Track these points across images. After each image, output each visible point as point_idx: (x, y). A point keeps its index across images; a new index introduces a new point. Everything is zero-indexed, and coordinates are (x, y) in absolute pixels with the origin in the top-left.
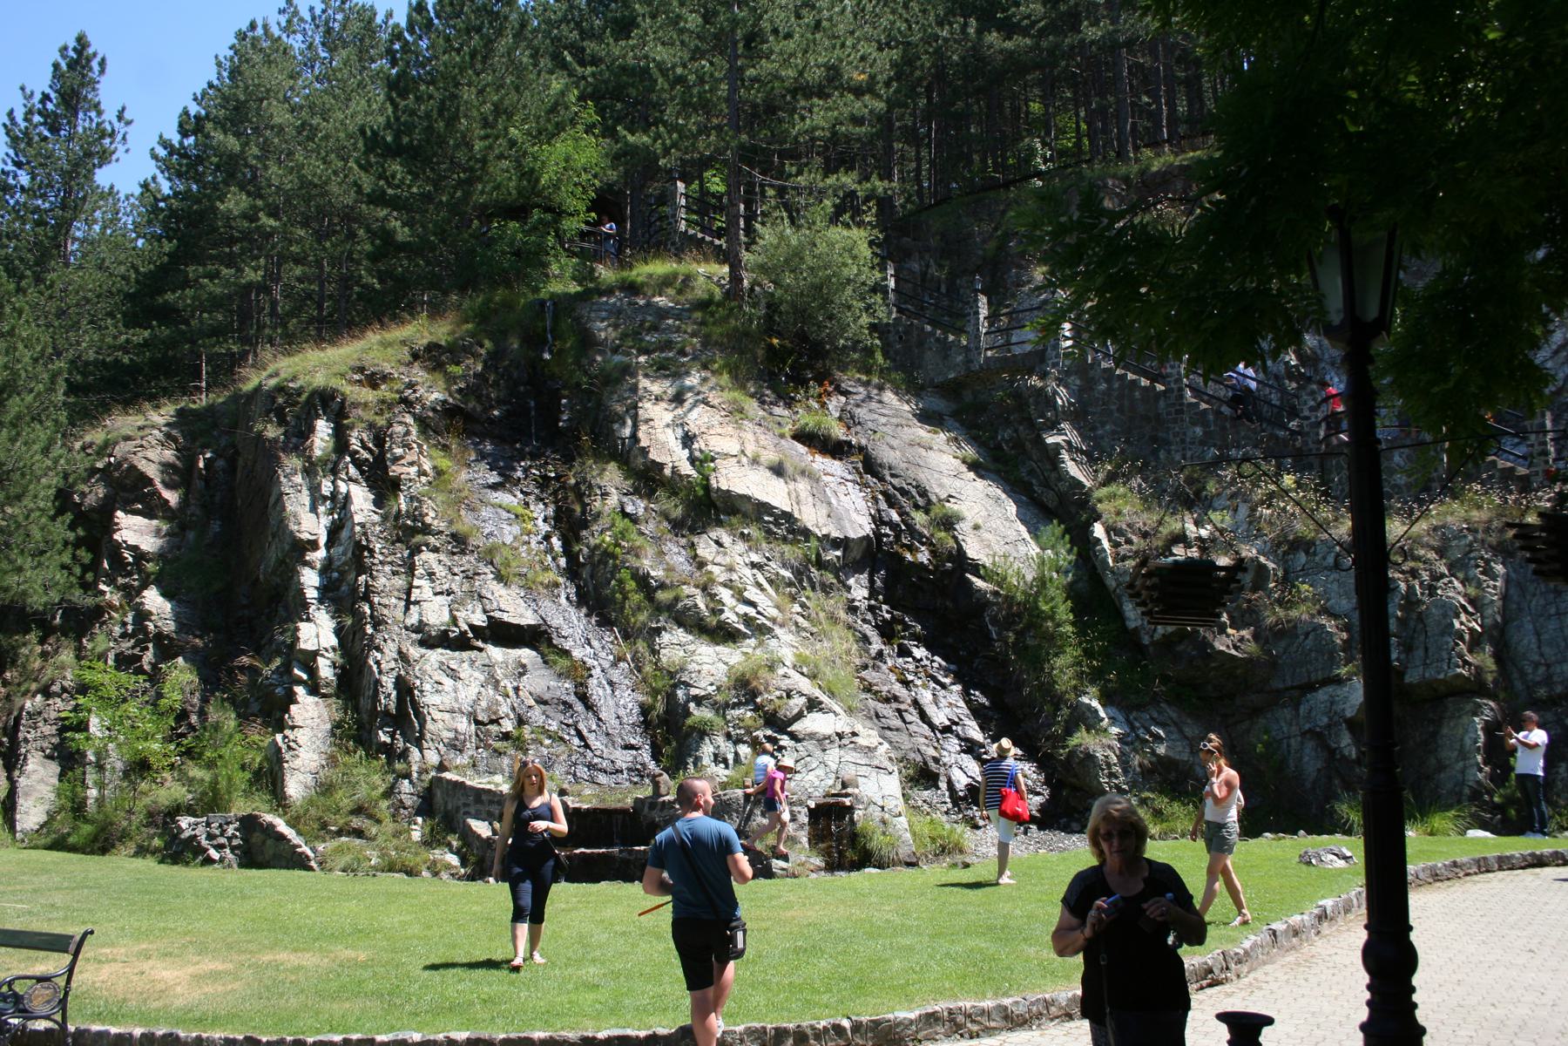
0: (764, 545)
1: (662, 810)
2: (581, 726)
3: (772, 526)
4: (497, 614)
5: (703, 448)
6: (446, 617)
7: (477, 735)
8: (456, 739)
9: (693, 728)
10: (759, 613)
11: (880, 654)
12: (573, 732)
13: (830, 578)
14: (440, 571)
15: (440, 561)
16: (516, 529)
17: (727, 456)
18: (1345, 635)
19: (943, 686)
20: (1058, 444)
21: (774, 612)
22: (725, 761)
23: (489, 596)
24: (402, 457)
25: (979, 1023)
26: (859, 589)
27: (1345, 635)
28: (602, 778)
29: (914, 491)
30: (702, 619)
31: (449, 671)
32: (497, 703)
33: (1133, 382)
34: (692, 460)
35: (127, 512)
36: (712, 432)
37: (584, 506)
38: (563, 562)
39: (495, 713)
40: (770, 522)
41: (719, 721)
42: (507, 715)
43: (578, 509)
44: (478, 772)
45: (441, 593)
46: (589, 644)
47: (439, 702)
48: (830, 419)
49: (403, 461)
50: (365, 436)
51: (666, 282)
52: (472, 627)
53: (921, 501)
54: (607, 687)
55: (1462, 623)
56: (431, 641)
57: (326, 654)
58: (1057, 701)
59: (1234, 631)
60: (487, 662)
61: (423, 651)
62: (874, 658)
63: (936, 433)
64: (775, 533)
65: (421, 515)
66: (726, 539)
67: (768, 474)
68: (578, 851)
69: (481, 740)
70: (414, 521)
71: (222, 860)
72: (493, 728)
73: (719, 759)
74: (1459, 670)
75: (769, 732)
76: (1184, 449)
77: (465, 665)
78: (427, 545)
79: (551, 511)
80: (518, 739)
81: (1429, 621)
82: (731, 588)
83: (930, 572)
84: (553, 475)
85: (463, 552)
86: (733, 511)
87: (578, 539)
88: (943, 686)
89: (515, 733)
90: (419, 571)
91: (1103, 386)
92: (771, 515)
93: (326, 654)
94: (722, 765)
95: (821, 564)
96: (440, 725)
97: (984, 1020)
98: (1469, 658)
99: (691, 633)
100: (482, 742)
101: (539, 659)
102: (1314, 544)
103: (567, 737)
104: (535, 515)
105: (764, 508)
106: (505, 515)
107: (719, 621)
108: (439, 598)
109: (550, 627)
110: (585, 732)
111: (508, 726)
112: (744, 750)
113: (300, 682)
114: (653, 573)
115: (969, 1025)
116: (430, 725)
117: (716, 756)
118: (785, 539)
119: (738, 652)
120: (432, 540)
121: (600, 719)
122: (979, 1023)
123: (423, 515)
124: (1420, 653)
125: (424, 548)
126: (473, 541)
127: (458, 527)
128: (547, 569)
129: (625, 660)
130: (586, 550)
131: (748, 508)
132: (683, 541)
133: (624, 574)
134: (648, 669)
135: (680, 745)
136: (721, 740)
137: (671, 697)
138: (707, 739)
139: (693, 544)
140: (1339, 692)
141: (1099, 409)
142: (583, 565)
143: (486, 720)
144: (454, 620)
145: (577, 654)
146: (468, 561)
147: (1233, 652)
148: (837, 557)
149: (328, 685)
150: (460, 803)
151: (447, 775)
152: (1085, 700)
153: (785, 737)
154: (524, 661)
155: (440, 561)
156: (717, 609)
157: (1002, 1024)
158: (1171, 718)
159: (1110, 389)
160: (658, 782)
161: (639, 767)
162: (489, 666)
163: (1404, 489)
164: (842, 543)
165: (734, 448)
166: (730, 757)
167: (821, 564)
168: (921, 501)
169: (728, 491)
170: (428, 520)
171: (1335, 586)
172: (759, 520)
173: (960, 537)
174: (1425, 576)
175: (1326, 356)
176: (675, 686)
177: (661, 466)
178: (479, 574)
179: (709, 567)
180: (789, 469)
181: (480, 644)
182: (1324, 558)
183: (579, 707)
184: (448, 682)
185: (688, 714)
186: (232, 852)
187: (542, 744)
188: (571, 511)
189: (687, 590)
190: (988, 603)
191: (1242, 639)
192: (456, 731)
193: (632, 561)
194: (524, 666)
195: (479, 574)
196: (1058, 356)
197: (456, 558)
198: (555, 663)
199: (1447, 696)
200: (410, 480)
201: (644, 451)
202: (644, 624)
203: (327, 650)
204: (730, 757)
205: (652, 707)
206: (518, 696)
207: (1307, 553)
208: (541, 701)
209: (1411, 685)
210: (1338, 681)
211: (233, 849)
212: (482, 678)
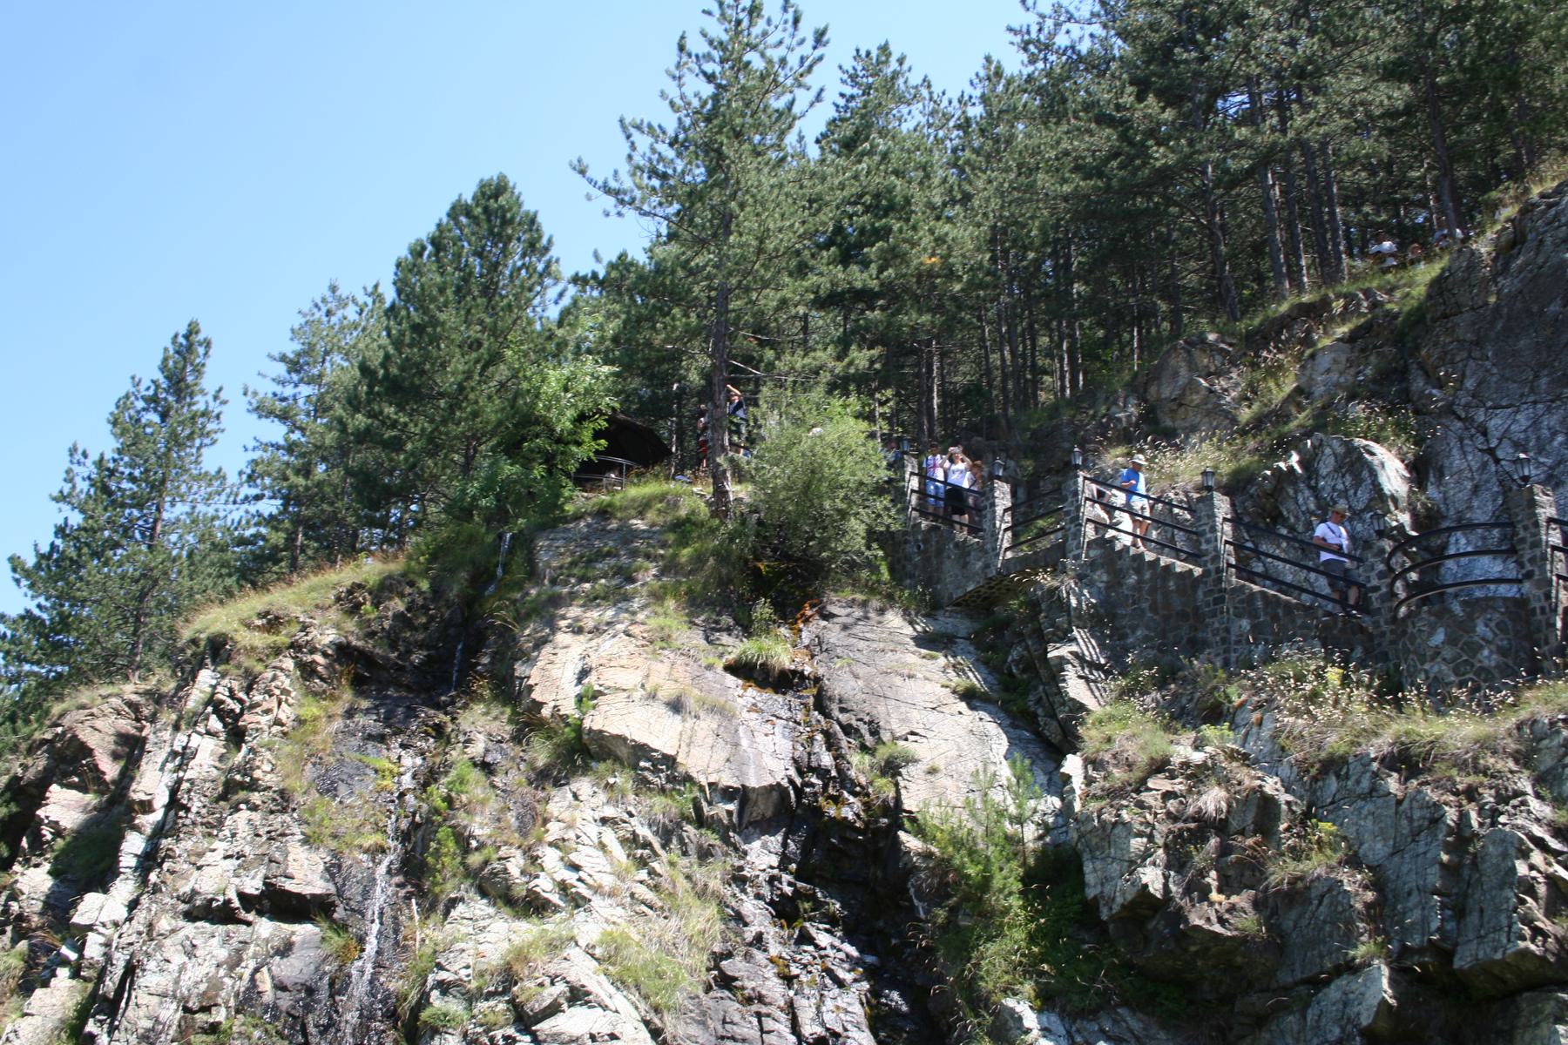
0: (631, 797)
3: (646, 773)
8: (153, 1029)
11: (759, 940)
13: (711, 838)
18: (1370, 896)
19: (840, 984)
20: (1061, 658)
24: (258, 705)
26: (763, 854)
27: (1370, 896)
29: (864, 729)
33: (1168, 568)
35: (63, 785)
45: (230, 857)
48: (781, 651)
50: (236, 685)
51: (643, 507)
52: (242, 896)
53: (869, 740)
55: (1532, 867)
57: (102, 930)
58: (979, 1002)
59: (1222, 897)
62: (750, 944)
63: (933, 658)
67: (663, 710)
74: (1522, 944)
76: (1226, 651)
78: (247, 802)
81: (1486, 866)
83: (858, 831)
88: (840, 984)
91: (1132, 579)
92: (649, 760)
93: (102, 930)
96: (142, 1012)
98: (1543, 923)
102: (1347, 763)
105: (642, 750)
113: (65, 962)
118: (663, 790)
124: (1474, 919)
131: (623, 752)
140: (1354, 987)
141: (1129, 610)
143: (196, 1007)
147: (1217, 928)
148: (729, 813)
152: (1010, 1002)
158: (1132, 1032)
159: (1140, 581)
163: (1496, 673)
164: (741, 795)
167: (701, 821)
168: (869, 740)
169: (601, 732)
170: (257, 774)
171: (1369, 822)
173: (902, 784)
174: (1488, 797)
175: (1452, 512)
180: (691, 703)
182: (1358, 782)
190: (914, 869)
191: (1232, 909)
196: (1079, 546)
199: (1519, 991)
203: (104, 925)
207: (1338, 776)
209: (1461, 970)
210: (1352, 968)
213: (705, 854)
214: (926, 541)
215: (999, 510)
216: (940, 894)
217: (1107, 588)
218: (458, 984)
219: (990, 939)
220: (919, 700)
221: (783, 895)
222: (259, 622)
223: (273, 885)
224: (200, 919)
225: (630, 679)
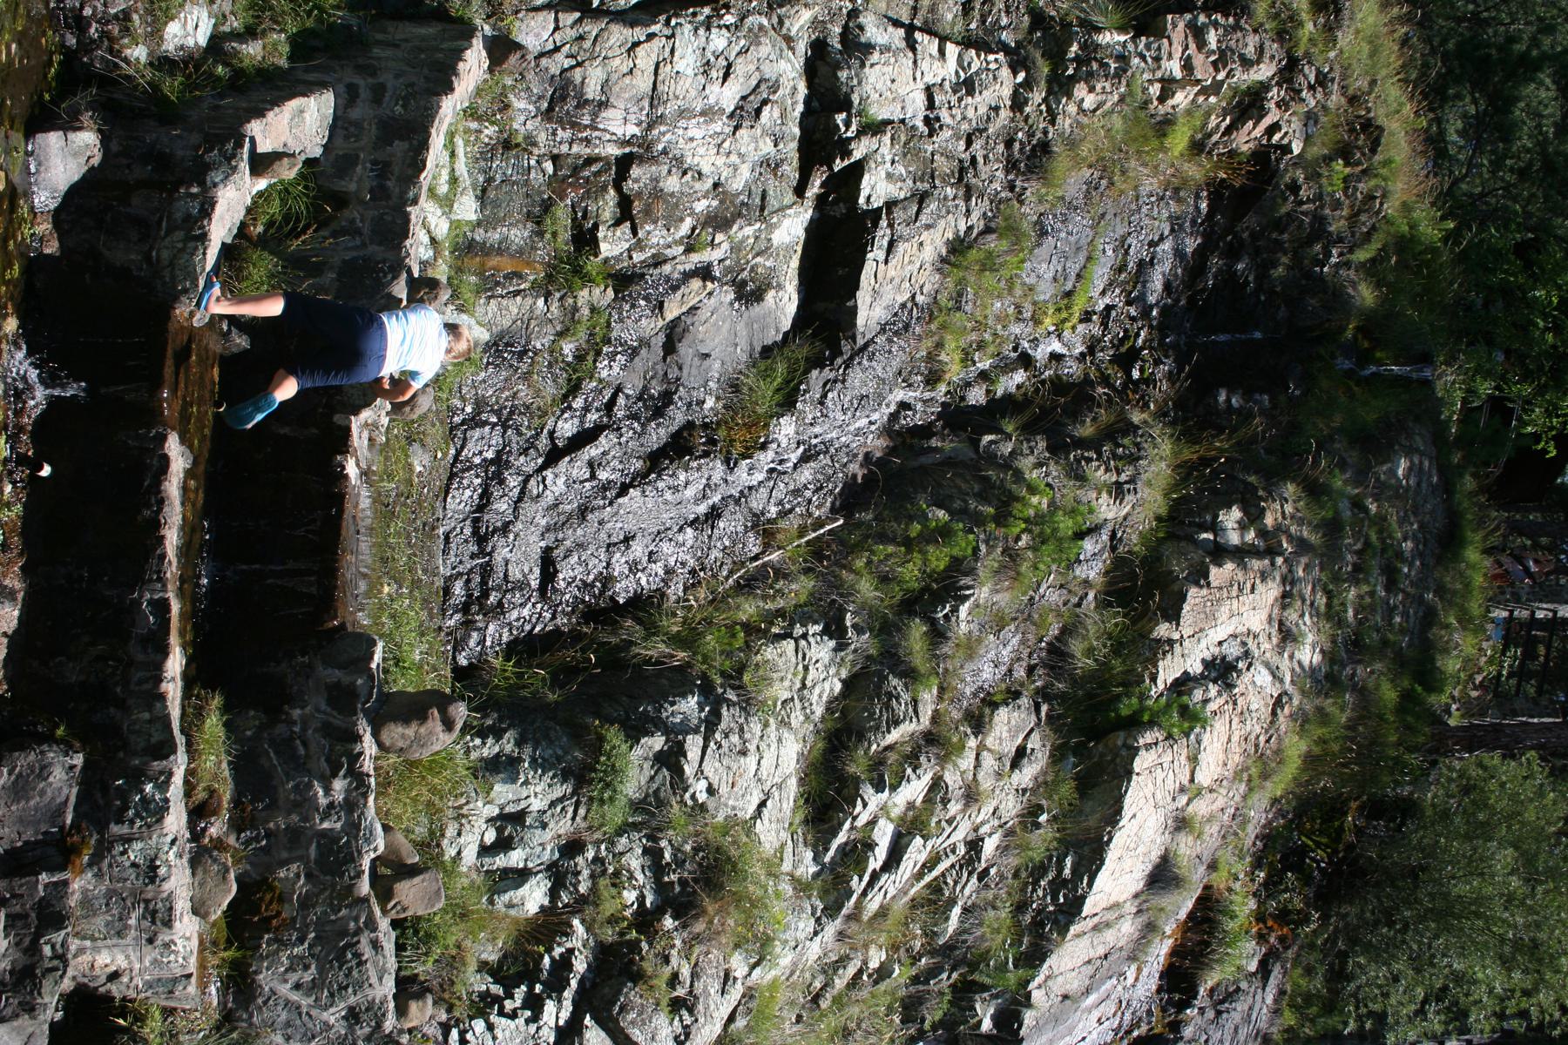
1: (327, 730)
2: (605, 442)
3: (1051, 875)
4: (882, 235)
5: (1212, 706)
6: (880, 112)
7: (590, 161)
8: (582, 103)
9: (597, 746)
10: (875, 876)
12: (593, 417)
14: (978, 105)
15: (996, 109)
16: (1046, 292)
17: (1194, 760)
21: (873, 904)
22: (503, 845)
23: (924, 219)
24: (1201, 44)
28: (462, 498)
30: (861, 736)
31: (755, 101)
32: (672, 221)
34: (1183, 684)
36: (1236, 720)
37: (1094, 444)
38: (977, 396)
39: (648, 212)
40: (1060, 869)
41: (616, 814)
42: (639, 245)
43: (1086, 430)
44: (488, 153)
45: (931, 105)
46: (805, 458)
47: (680, 65)
49: (1193, 46)
52: (857, 170)
54: (702, 509)
56: (823, 69)
60: (773, 203)
61: (802, 47)
64: (1036, 883)
65: (1091, 74)
66: (1026, 775)
67: (1155, 855)
68: (174, 447)
69: (576, 170)
70: (1077, 59)
72: (608, 205)
73: (511, 825)
75: (580, 965)
77: (767, 147)
78: (1028, 84)
79: (1072, 369)
80: (578, 271)
82: (928, 800)
84: (1136, 374)
85: (1011, 166)
86: (1085, 784)
87: (1028, 430)
89: (592, 265)
90: (975, 61)
94: (490, 837)
95: (965, 992)
96: (620, 64)
97: (461, 569)
99: (829, 709)
100: (570, 173)
101: (773, 336)
103: (578, 403)
104: (1067, 334)
105: (1091, 855)
106: (1073, 268)
107: (856, 782)
108: (920, 99)
109: (848, 364)
110: (592, 451)
111: (612, 245)
112: (533, 897)
114: (964, 610)
116: (619, 35)
117: (518, 818)
118: (1020, 907)
119: (784, 835)
120: (1037, 96)
121: (623, 490)
123: (1089, 78)
125: (1021, 77)
126: (1032, 189)
127: (1061, 160)
128: (967, 359)
129: (767, 547)
130: (1007, 448)
132: (1020, 672)
133: (962, 544)
134: (748, 609)
135: (550, 711)
136: (562, 826)
137: (679, 681)
138: (568, 788)
139: (1016, 695)
142: (975, 443)
143: (630, 186)
144: (874, 128)
145: (786, 429)
146: (992, 175)
150: (387, 78)
151: (474, 63)
153: (565, 1015)
154: (770, 296)
155: (996, 109)
156: (884, 775)
160: (423, 718)
161: (493, 598)
162: (759, 208)
165: (1204, 777)
166: (515, 858)
167: (965, 992)
169: (1129, 773)
170: (1080, 90)
172: (1066, 844)
176: (707, 690)
177: (1174, 616)
178: (967, 198)
179: (972, 743)
181: (814, 189)
183: (657, 435)
184: (728, 96)
185: (635, 733)
187: (561, 335)
188: (1075, 415)
189: (928, 698)
192: (603, 105)
193: (990, 560)
194: (757, 296)
195: (967, 198)
197: (1001, 148)
198: (766, 375)
200: (1157, 59)
201: (1199, 576)
202: (849, 594)
204: (515, 858)
205: (651, 629)
206: (687, 276)
208: (673, 336)
212: (737, 185)
218: (679, 781)
223: (876, 225)
224: (810, 86)
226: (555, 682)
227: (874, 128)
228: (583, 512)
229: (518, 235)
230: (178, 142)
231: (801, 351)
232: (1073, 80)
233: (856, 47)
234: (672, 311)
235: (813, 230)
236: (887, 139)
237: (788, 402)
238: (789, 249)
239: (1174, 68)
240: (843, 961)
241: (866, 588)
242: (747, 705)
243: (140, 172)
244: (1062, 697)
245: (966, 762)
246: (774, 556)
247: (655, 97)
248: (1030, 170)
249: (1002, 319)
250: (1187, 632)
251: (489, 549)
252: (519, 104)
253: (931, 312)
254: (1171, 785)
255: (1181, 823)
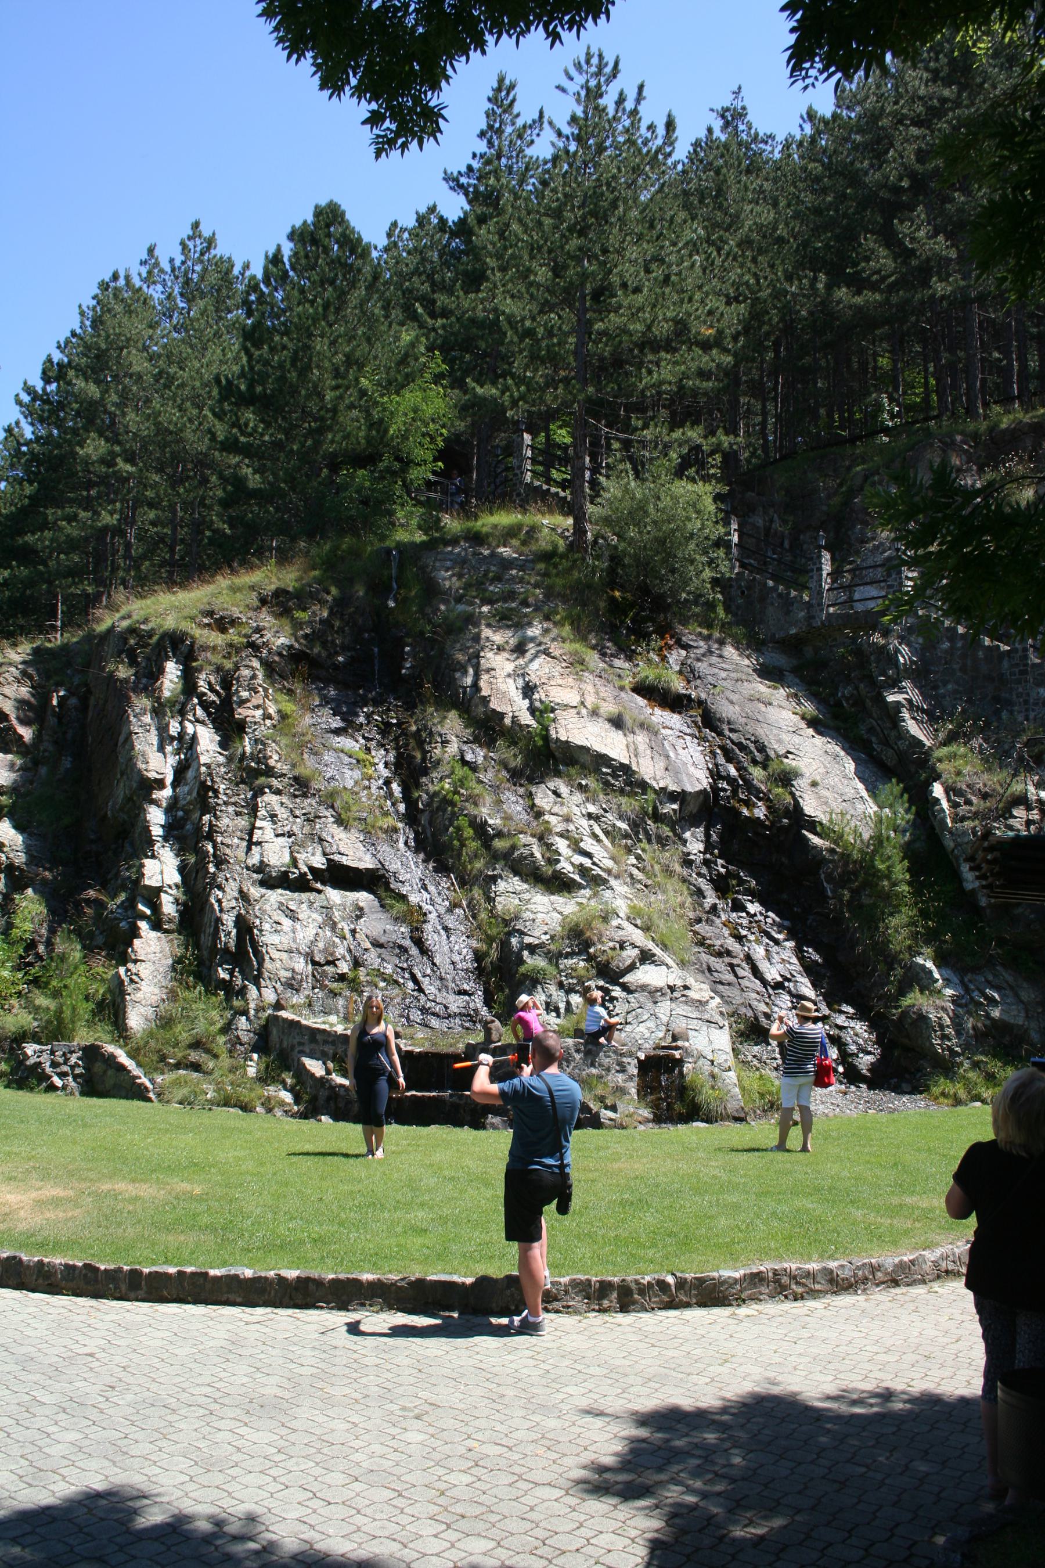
3: (609, 778)
4: (337, 857)
5: (543, 698)
6: (287, 859)
7: (314, 976)
8: (293, 978)
9: (525, 976)
10: (594, 864)
12: (407, 975)
14: (282, 813)
16: (357, 774)
17: (566, 707)
19: (777, 942)
20: (898, 702)
21: (609, 863)
22: (557, 1010)
24: (248, 700)
25: (804, 1285)
26: (695, 844)
28: (434, 1022)
29: (752, 746)
30: (538, 868)
31: (287, 912)
32: (335, 945)
34: (532, 710)
37: (425, 752)
38: (402, 807)
39: (332, 954)
40: (607, 774)
41: (551, 970)
42: (344, 957)
43: (418, 756)
44: (313, 1012)
45: (283, 835)
46: (426, 890)
49: (248, 705)
50: (212, 678)
51: (511, 532)
52: (312, 869)
53: (759, 757)
54: (442, 932)
56: (272, 882)
60: (325, 903)
61: (263, 891)
62: (708, 912)
63: (776, 688)
66: (564, 790)
67: (607, 726)
69: (317, 981)
71: (64, 1087)
72: (329, 969)
75: (601, 983)
76: (1027, 710)
78: (270, 787)
79: (391, 757)
80: (354, 980)
82: (567, 838)
83: (767, 828)
84: (394, 721)
85: (305, 795)
87: (418, 785)
88: (777, 942)
89: (351, 975)
90: (262, 813)
91: (946, 645)
94: (554, 1014)
95: (657, 817)
96: (278, 964)
99: (526, 882)
100: (318, 982)
101: (376, 903)
103: (401, 981)
105: (603, 759)
107: (555, 871)
108: (281, 839)
110: (419, 976)
111: (344, 967)
113: (143, 917)
114: (491, 822)
115: (794, 1287)
116: (268, 964)
117: (547, 1004)
118: (622, 792)
120: (275, 782)
121: (434, 964)
122: (804, 1285)
126: (315, 785)
128: (386, 814)
129: (460, 906)
130: (425, 796)
134: (483, 916)
136: (553, 989)
137: (505, 944)
138: (539, 987)
139: (531, 794)
142: (422, 811)
143: (322, 961)
144: (294, 862)
145: (414, 899)
146: (309, 804)
149: (170, 921)
150: (295, 1042)
152: (920, 960)
153: (617, 988)
154: (361, 904)
157: (827, 1287)
159: (952, 648)
162: (327, 908)
164: (680, 797)
166: (562, 1006)
167: (657, 817)
169: (567, 742)
170: (272, 763)
172: (597, 771)
173: (798, 793)
177: (501, 716)
178: (320, 817)
179: (547, 817)
180: (628, 721)
181: (319, 886)
183: (414, 951)
184: (287, 923)
185: (522, 962)
186: (75, 1080)
189: (523, 839)
190: (823, 861)
192: (293, 971)
193: (471, 809)
194: (361, 909)
197: (298, 800)
198: (392, 907)
200: (255, 723)
202: (481, 872)
203: (170, 887)
204: (562, 1006)
205: (486, 954)
206: (354, 939)
208: (377, 944)
211: (75, 1077)
212: (320, 919)
213: (662, 842)
214: (749, 588)
215: (824, 573)
216: (843, 881)
217: (922, 649)
218: (541, 945)
219: (892, 914)
220: (782, 724)
221: (719, 874)
222: (206, 621)
225: (573, 699)
226: (502, 990)
227: (294, 862)
228: (441, 979)
229: (341, 1002)
230: (323, 1094)
231: (381, 892)
232: (267, 765)
233: (260, 868)
234: (368, 945)
235: (335, 886)
236: (298, 856)
237: (403, 898)
238: (342, 897)
239: (259, 713)
240: (631, 876)
241: (479, 865)
242: (517, 918)
243: (332, 1104)
244: (533, 771)
245: (553, 820)
246: (464, 903)
247: (290, 951)
248: (307, 787)
249: (370, 796)
250: (509, 709)
251: (228, 934)
252: (294, 1001)
253: (367, 833)
254: (575, 720)
255: (594, 713)
